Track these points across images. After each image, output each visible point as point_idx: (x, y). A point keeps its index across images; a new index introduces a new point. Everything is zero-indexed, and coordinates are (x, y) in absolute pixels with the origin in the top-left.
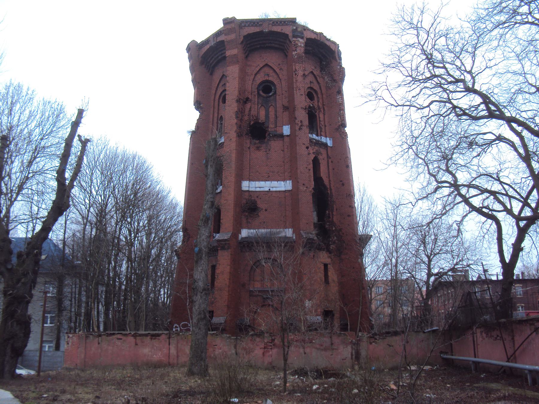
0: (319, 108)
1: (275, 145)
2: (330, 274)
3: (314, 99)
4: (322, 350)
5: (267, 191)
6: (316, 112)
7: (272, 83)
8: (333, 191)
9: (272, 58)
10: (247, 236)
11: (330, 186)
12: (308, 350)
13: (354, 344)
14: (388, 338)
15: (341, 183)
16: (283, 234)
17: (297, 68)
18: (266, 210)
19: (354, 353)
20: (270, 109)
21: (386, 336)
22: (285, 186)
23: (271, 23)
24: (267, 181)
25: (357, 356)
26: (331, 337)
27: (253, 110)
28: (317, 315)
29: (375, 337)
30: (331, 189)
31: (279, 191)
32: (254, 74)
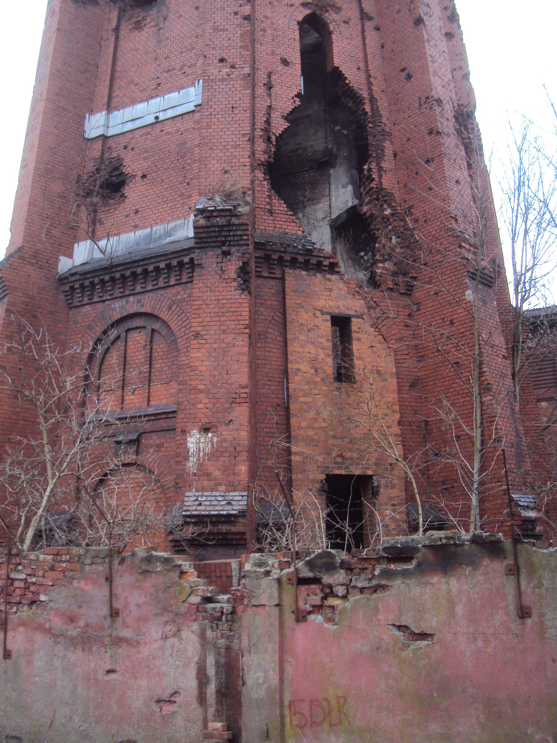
4: (73, 642)
8: (383, 104)
11: (370, 90)
13: (216, 619)
14: (398, 583)
15: (404, 74)
18: (144, 176)
19: (211, 671)
21: (386, 574)
29: (327, 579)
30: (373, 100)
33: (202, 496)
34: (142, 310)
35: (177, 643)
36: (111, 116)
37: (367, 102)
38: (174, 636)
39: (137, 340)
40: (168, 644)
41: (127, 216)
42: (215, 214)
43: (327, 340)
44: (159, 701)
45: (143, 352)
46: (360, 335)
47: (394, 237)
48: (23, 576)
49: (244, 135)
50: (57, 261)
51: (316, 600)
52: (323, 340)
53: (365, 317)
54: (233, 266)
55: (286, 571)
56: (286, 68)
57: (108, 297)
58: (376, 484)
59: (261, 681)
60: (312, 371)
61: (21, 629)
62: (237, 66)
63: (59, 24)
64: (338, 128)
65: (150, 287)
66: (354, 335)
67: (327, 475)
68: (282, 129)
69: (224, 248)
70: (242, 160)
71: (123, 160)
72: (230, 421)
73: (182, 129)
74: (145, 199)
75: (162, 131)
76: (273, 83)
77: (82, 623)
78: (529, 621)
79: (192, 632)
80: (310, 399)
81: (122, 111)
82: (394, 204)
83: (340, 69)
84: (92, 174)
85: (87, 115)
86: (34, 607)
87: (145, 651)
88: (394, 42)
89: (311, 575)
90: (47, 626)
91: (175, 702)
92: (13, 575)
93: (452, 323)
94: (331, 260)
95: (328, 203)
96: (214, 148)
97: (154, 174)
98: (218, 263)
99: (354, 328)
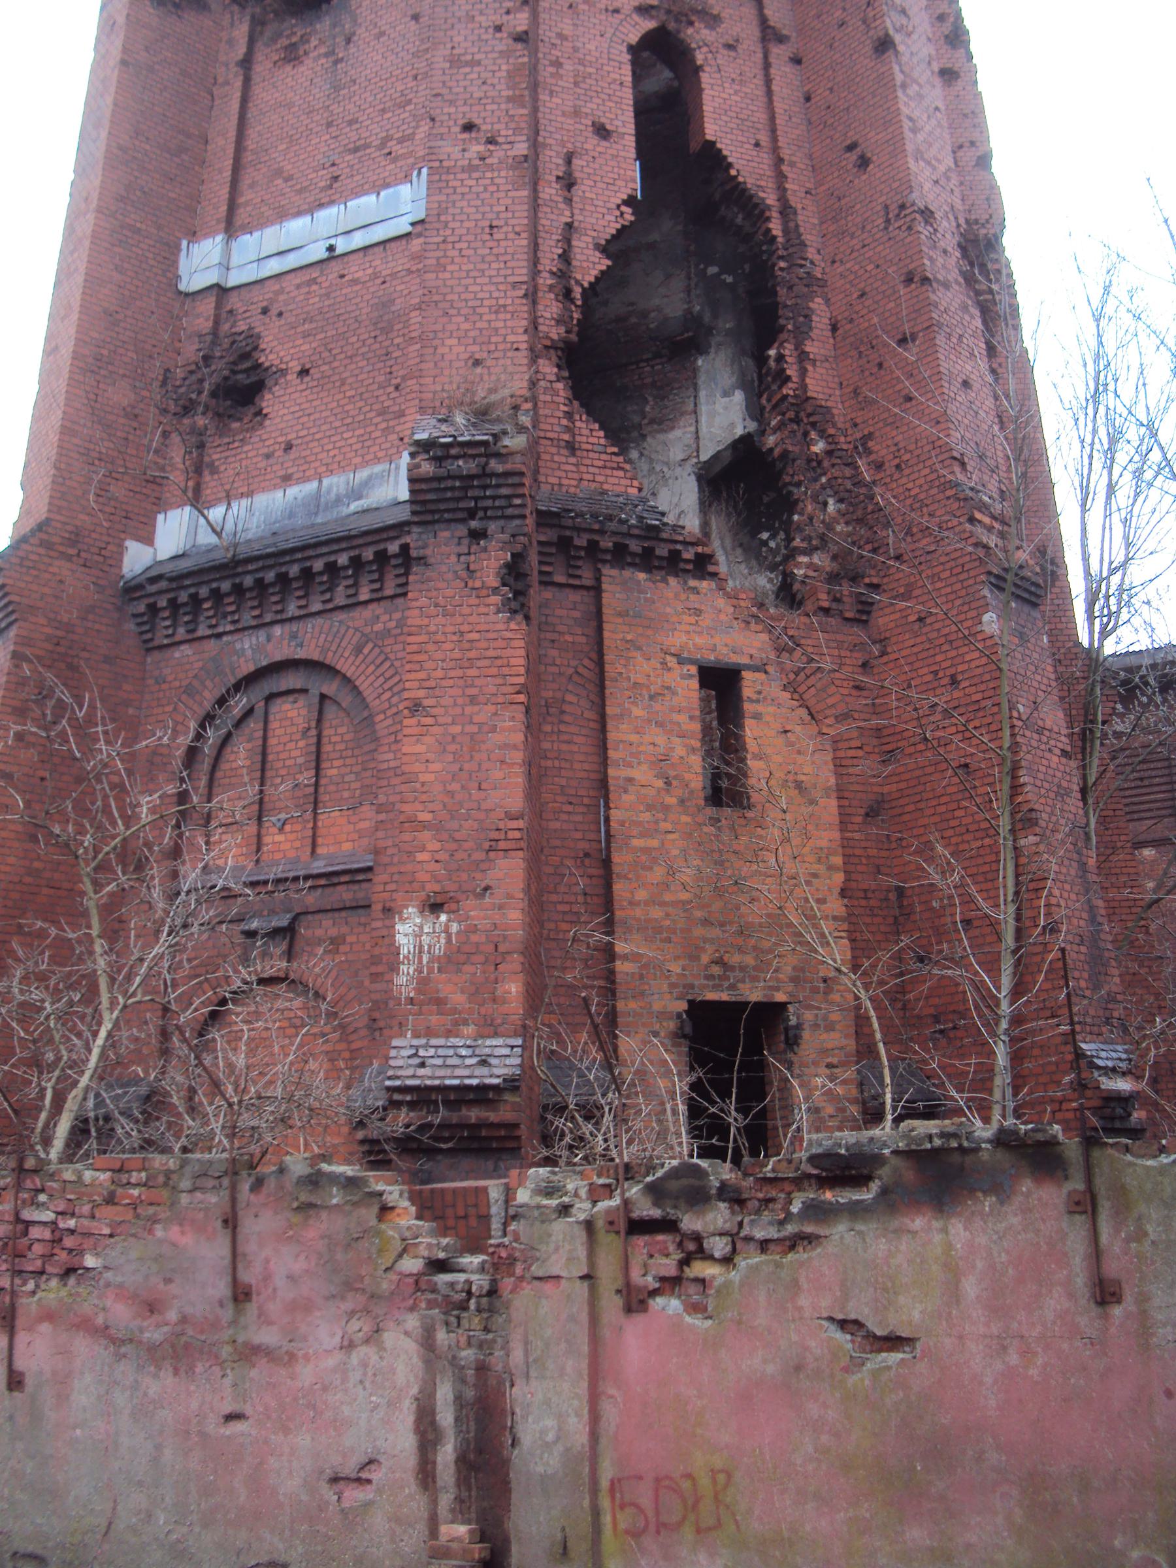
4: (154, 1354)
8: (808, 219)
11: (781, 190)
13: (456, 1307)
14: (839, 1231)
15: (853, 157)
18: (304, 372)
19: (446, 1417)
21: (815, 1211)
29: (690, 1222)
30: (787, 211)
33: (426, 1046)
34: (300, 654)
35: (374, 1358)
36: (234, 245)
37: (775, 214)
38: (367, 1341)
39: (290, 717)
40: (355, 1359)
41: (268, 456)
42: (453, 452)
43: (691, 718)
44: (335, 1480)
45: (301, 744)
46: (759, 708)
47: (831, 501)
48: (48, 1216)
49: (515, 285)
51: (667, 1265)
52: (682, 718)
53: (770, 669)
54: (491, 562)
55: (603, 1205)
56: (604, 143)
57: (229, 628)
58: (793, 1021)
59: (550, 1437)
60: (660, 784)
61: (45, 1327)
62: (500, 140)
64: (713, 270)
65: (316, 607)
66: (747, 706)
67: (691, 1003)
68: (595, 273)
69: (474, 524)
70: (511, 338)
71: (259, 337)
72: (486, 889)
73: (384, 273)
74: (305, 419)
75: (342, 276)
76: (577, 174)
77: (172, 1316)
78: (1117, 1311)
79: (406, 1333)
80: (655, 843)
81: (257, 234)
82: (831, 431)
83: (719, 146)
84: (193, 367)
85: (184, 243)
86: (72, 1281)
87: (306, 1374)
88: (831, 89)
89: (656, 1213)
90: (100, 1320)
91: (369, 1481)
92: (27, 1214)
93: (954, 681)
94: (700, 549)
95: (693, 429)
96: (452, 312)
97: (326, 368)
98: (459, 555)
99: (747, 692)
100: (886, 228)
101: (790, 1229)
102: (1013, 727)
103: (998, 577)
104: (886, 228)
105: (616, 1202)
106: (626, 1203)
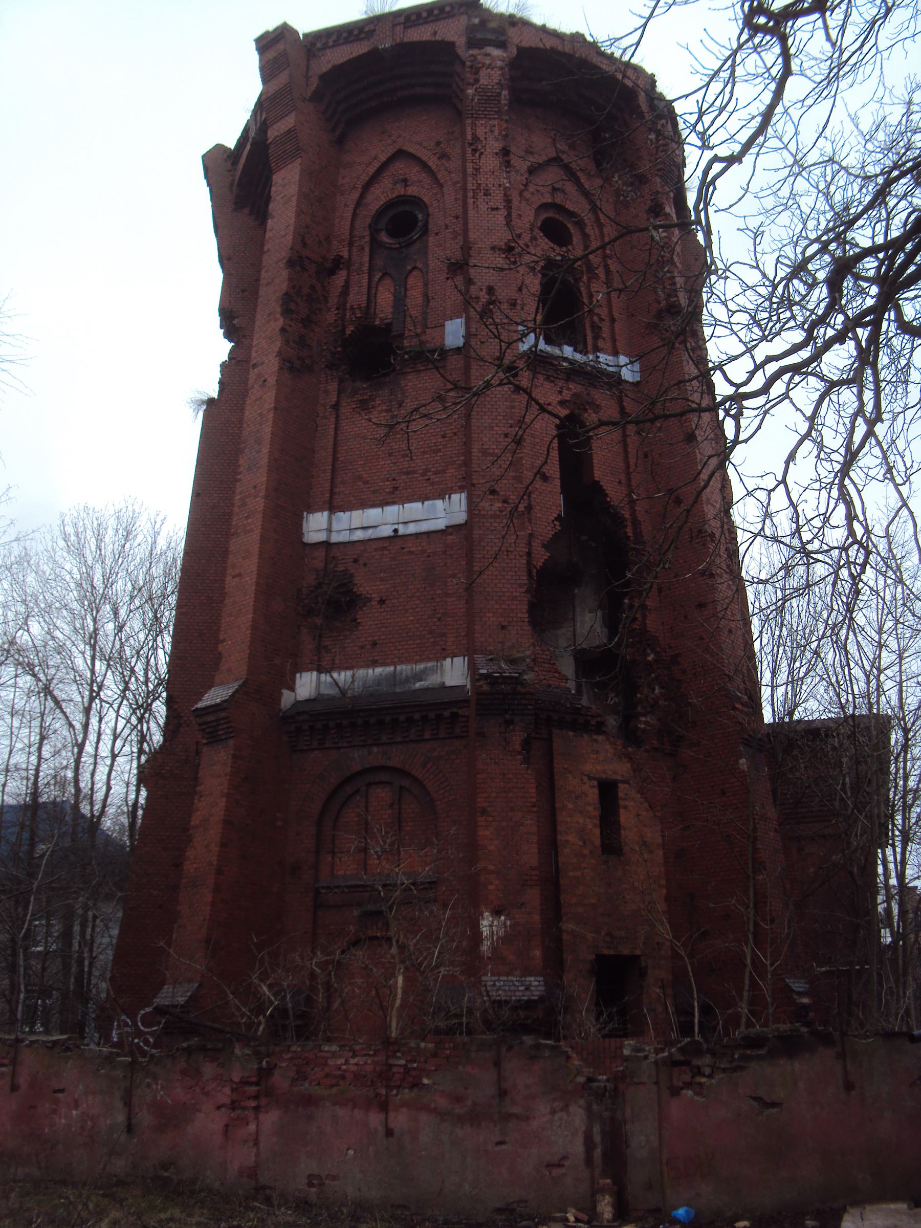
0: (590, 269)
1: (419, 386)
2: (625, 818)
3: (571, 243)
5: (389, 538)
6: (578, 280)
7: (416, 202)
9: (418, 133)
10: (313, 694)
11: (633, 512)
12: (400, 1120)
16: (433, 680)
17: (480, 132)
19: (597, 1138)
20: (411, 281)
22: (444, 512)
23: (402, 19)
24: (388, 504)
25: (612, 1153)
26: (497, 1064)
27: (354, 290)
28: (527, 972)
29: (696, 1062)
30: (636, 523)
31: (428, 534)
32: (359, 186)
33: (499, 980)
34: (390, 764)
35: (565, 1116)
36: (333, 517)
37: (629, 524)
38: (562, 1110)
39: (382, 795)
40: (557, 1117)
41: (362, 647)
42: (500, 681)
43: (595, 809)
44: (548, 1166)
45: (389, 812)
46: (627, 803)
47: (657, 688)
48: (403, 1062)
49: (520, 585)
50: (281, 694)
51: (687, 1078)
52: (591, 809)
53: (631, 782)
54: (517, 738)
55: (661, 1055)
56: (545, 484)
57: (345, 745)
58: (643, 964)
59: (643, 1143)
60: (581, 843)
61: (404, 1110)
62: (510, 501)
63: (277, 400)
64: (584, 538)
65: (399, 739)
66: (621, 802)
67: (597, 955)
68: (542, 561)
69: (507, 717)
70: (519, 615)
71: (352, 576)
72: (523, 904)
73: (429, 551)
74: (383, 629)
75: (403, 548)
76: (533, 503)
77: (469, 1103)
78: (853, 1093)
79: (580, 1107)
80: (579, 874)
81: (348, 513)
82: (658, 649)
83: (601, 483)
84: (313, 589)
85: (305, 513)
86: (416, 1090)
87: (535, 1124)
88: (660, 455)
89: (682, 1058)
90: (433, 1105)
91: (563, 1165)
92: (391, 1061)
93: (723, 793)
94: (599, 719)
95: (571, 629)
96: (489, 598)
97: (396, 601)
98: (500, 733)
99: (621, 795)
100: (691, 542)
101: (735, 1064)
102: (754, 819)
103: (747, 739)
104: (691, 542)
105: (666, 1054)
106: (671, 1054)
